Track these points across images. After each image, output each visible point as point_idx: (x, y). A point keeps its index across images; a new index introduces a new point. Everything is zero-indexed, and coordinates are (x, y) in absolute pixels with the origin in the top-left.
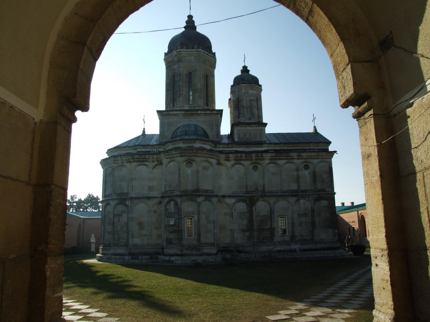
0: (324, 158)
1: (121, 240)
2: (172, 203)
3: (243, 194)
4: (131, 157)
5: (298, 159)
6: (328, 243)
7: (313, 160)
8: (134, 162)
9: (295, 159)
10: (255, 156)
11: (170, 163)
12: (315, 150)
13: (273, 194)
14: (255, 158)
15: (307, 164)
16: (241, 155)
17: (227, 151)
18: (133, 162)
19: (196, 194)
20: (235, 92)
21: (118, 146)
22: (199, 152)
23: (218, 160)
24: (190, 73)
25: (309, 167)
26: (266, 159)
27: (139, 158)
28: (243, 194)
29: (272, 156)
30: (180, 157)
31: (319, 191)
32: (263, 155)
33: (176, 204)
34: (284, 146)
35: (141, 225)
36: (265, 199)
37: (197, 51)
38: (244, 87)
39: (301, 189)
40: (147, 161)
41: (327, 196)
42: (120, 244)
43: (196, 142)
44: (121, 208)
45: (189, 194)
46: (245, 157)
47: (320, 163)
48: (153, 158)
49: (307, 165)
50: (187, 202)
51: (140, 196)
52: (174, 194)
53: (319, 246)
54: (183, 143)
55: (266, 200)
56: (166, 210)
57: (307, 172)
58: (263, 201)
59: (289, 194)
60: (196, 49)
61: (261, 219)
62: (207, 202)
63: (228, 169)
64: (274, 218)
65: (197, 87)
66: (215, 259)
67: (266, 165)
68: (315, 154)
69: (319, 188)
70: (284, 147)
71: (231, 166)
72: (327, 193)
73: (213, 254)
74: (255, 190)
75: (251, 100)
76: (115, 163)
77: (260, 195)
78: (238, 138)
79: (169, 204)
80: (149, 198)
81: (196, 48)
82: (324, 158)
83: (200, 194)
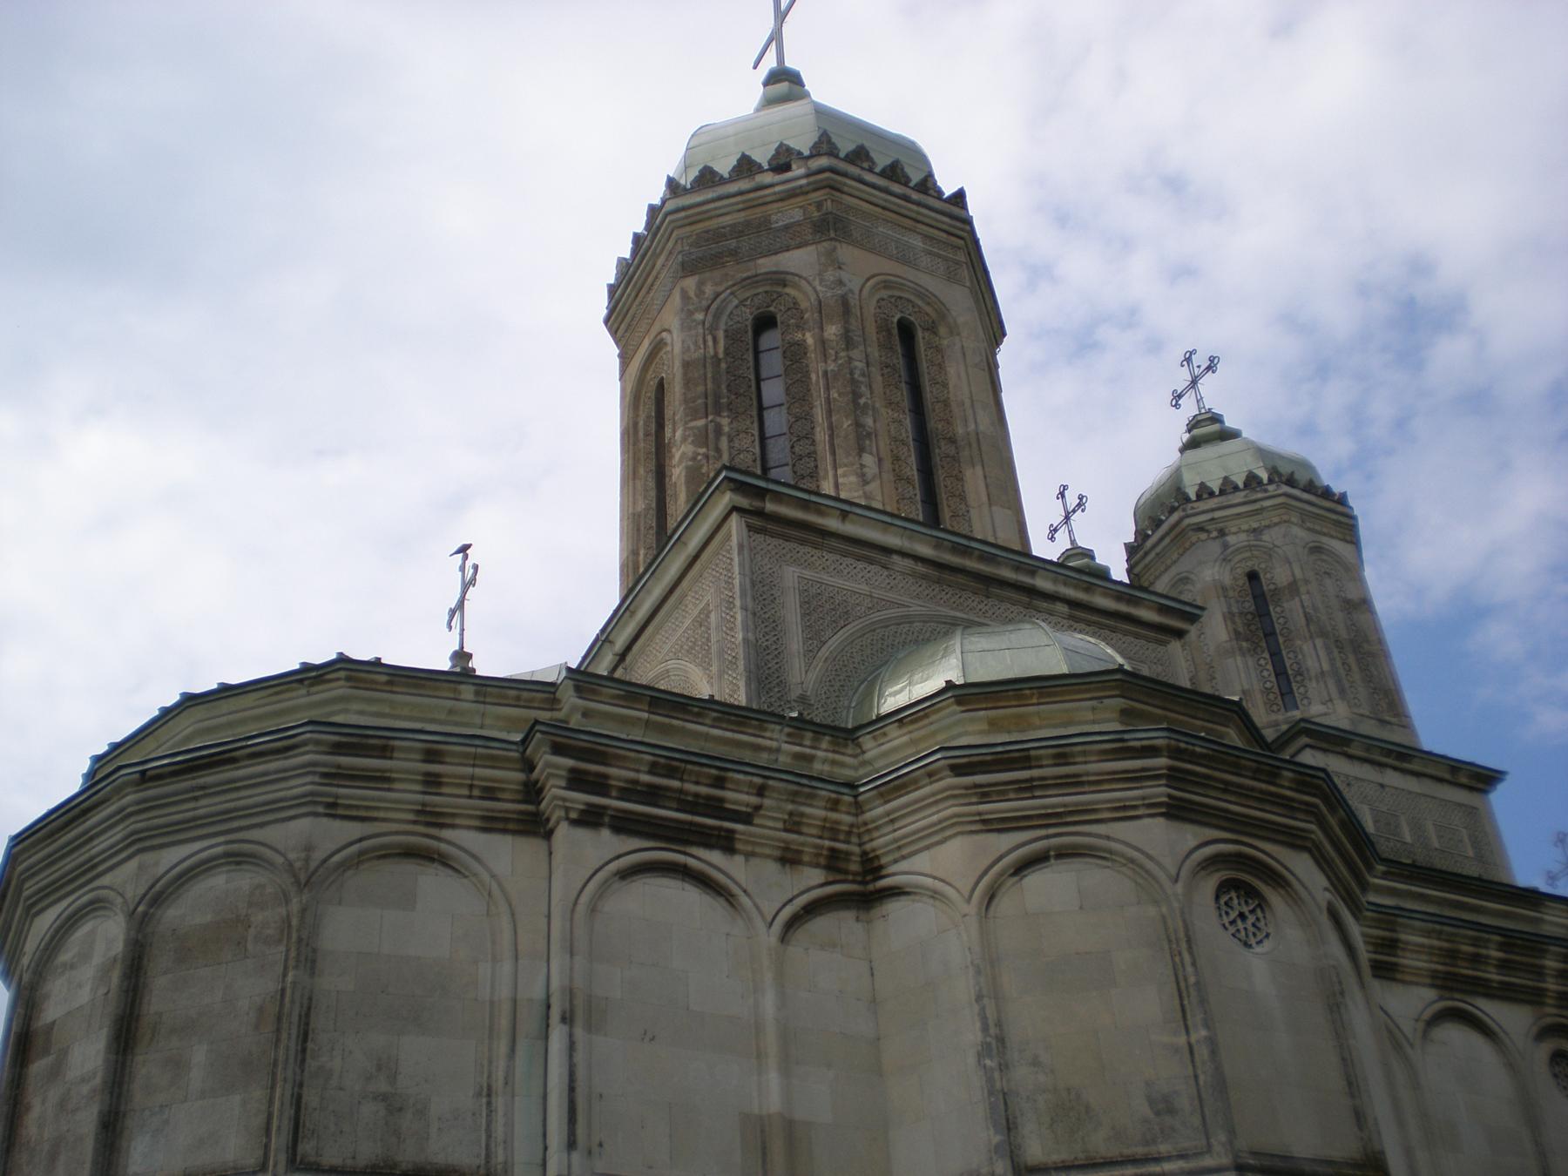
8: (590, 819)
11: (1036, 880)
18: (576, 823)
20: (1222, 533)
21: (159, 752)
40: (726, 843)
65: (972, 427)
76: (333, 809)
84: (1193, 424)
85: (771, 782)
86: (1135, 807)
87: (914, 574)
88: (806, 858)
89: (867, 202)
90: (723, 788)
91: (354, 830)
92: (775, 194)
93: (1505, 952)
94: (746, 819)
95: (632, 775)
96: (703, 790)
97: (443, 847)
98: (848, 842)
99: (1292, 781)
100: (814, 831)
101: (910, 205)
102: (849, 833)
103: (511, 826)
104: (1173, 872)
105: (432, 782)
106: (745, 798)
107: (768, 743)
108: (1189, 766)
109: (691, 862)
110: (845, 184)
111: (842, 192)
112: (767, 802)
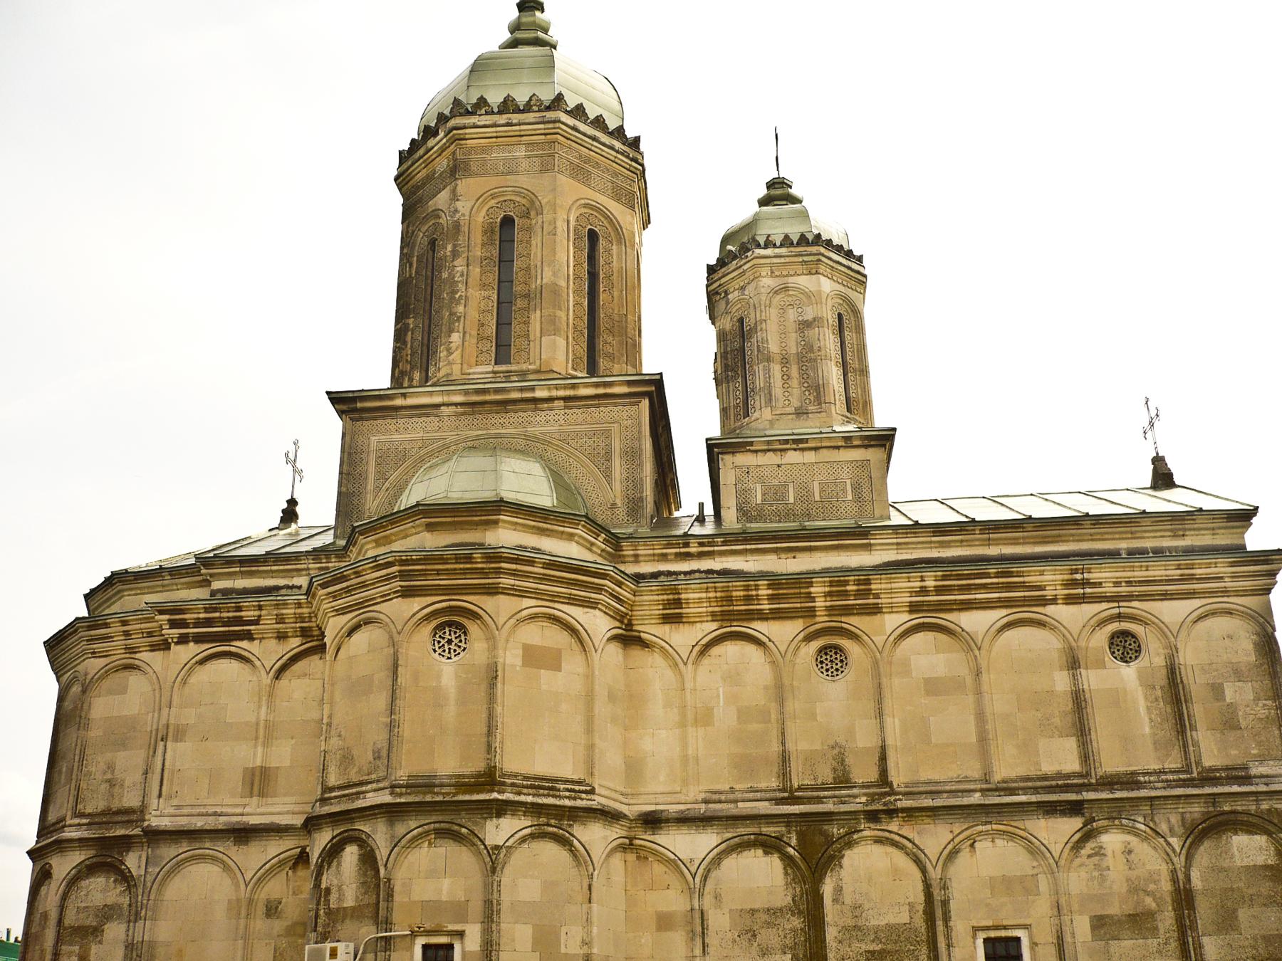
2: (351, 854)
3: (765, 808)
5: (1071, 600)
6: (977, 543)
8: (183, 640)
9: (1054, 601)
10: (827, 589)
11: (357, 637)
13: (939, 802)
14: (828, 604)
15: (1126, 626)
16: (747, 588)
18: (177, 643)
19: (476, 797)
20: (726, 293)
22: (503, 565)
23: (622, 622)
24: (507, 222)
25: (1139, 646)
26: (893, 609)
28: (766, 803)
29: (923, 591)
30: (403, 596)
31: (1209, 777)
32: (873, 587)
33: (369, 859)
36: (890, 832)
37: (541, 120)
38: (768, 261)
39: (1100, 773)
40: (249, 636)
41: (1265, 806)
43: (496, 522)
44: (100, 890)
45: (440, 798)
46: (772, 598)
47: (1200, 618)
49: (1125, 634)
51: (199, 823)
52: (360, 803)
54: (430, 527)
55: (897, 838)
56: (320, 894)
57: (1129, 673)
58: (878, 841)
59: (1034, 798)
60: (539, 111)
61: (872, 947)
62: (549, 850)
64: (949, 946)
67: (892, 638)
69: (1208, 762)
71: (697, 649)
72: (1263, 788)
74: (831, 780)
75: (805, 325)
77: (860, 807)
78: (740, 509)
79: (335, 864)
80: (243, 834)
81: (535, 108)
83: (500, 797)
84: (770, 185)
85: (262, 603)
86: (389, 594)
87: (457, 415)
88: (290, 634)
90: (242, 611)
91: (103, 661)
92: (435, 152)
93: (773, 589)
94: (256, 622)
95: (196, 616)
96: (231, 614)
97: (137, 662)
98: (310, 621)
99: (482, 558)
100: (291, 620)
101: (514, 128)
102: (310, 617)
103: (162, 647)
104: (399, 628)
105: (127, 634)
106: (252, 613)
107: (303, 566)
108: (410, 568)
109: (233, 649)
110: (466, 134)
111: (466, 139)
112: (263, 612)
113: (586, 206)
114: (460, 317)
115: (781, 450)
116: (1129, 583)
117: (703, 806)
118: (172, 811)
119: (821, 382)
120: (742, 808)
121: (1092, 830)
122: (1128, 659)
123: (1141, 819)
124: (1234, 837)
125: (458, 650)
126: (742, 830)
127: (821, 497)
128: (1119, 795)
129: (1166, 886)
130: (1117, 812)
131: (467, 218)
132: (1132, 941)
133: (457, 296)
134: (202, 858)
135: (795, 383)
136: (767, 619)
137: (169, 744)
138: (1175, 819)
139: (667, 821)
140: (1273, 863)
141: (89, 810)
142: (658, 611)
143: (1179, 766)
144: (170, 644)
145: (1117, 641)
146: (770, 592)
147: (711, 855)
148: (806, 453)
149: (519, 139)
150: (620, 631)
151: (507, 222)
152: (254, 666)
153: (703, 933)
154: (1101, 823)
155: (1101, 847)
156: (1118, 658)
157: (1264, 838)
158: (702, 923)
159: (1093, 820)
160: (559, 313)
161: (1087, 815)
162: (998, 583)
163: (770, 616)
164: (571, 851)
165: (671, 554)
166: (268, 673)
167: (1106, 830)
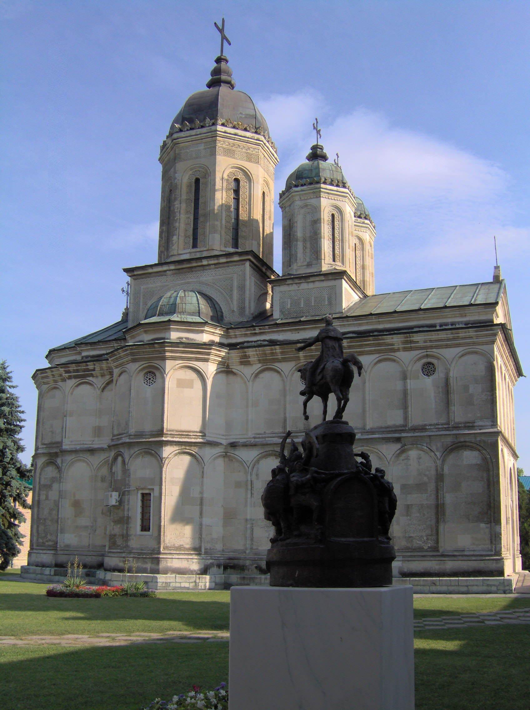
0: (474, 344)
1: (49, 537)
4: (63, 369)
5: (405, 349)
7: (445, 349)
8: (70, 378)
9: (398, 350)
12: (457, 326)
14: (304, 354)
16: (272, 350)
17: (252, 342)
23: (224, 365)
27: (77, 371)
28: (277, 438)
34: (380, 320)
35: (77, 504)
38: (298, 193)
40: (92, 375)
41: (478, 439)
42: (47, 543)
46: (282, 353)
47: (462, 356)
48: (101, 369)
49: (430, 363)
50: (141, 456)
51: (78, 447)
52: (120, 442)
53: (450, 565)
57: (428, 381)
59: (381, 436)
60: (209, 126)
63: (247, 382)
66: (195, 582)
68: (448, 336)
69: (457, 420)
70: (379, 323)
71: (254, 375)
73: (191, 572)
79: (116, 463)
80: (92, 451)
82: (474, 344)
87: (174, 274)
88: (106, 374)
89: (187, 142)
91: (47, 386)
93: (282, 349)
94: (94, 370)
96: (84, 367)
109: (87, 381)
110: (178, 141)
112: (95, 366)
113: (232, 168)
114: (177, 228)
115: (299, 283)
116: (431, 341)
117: (253, 440)
118: (69, 443)
119: (318, 250)
120: (268, 441)
121: (405, 449)
122: (430, 375)
123: (425, 445)
124: (464, 452)
125: (153, 382)
126: (267, 449)
127: (314, 304)
128: (416, 434)
129: (433, 472)
130: (416, 442)
131: (180, 181)
132: (417, 495)
133: (176, 219)
134: (80, 460)
135: (308, 250)
136: (280, 362)
137: (68, 418)
138: (439, 445)
139: (239, 446)
140: (479, 463)
141: (46, 443)
142: (238, 360)
143: (445, 421)
144: (66, 379)
145: (426, 367)
146: (281, 350)
147: (255, 459)
148: (309, 284)
149: (201, 140)
150: (223, 369)
151: (197, 181)
152: (94, 386)
153: (251, 489)
154: (408, 446)
155: (409, 456)
156: (434, 372)
157: (478, 452)
158: (251, 485)
159: (405, 445)
160: (216, 223)
161: (403, 443)
162: (374, 343)
163: (282, 360)
164: (195, 458)
165: (249, 334)
166: (99, 390)
167: (410, 449)
